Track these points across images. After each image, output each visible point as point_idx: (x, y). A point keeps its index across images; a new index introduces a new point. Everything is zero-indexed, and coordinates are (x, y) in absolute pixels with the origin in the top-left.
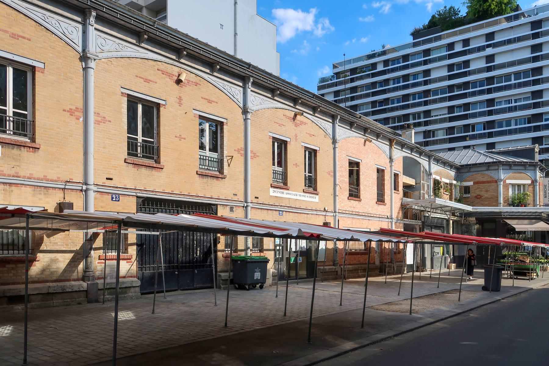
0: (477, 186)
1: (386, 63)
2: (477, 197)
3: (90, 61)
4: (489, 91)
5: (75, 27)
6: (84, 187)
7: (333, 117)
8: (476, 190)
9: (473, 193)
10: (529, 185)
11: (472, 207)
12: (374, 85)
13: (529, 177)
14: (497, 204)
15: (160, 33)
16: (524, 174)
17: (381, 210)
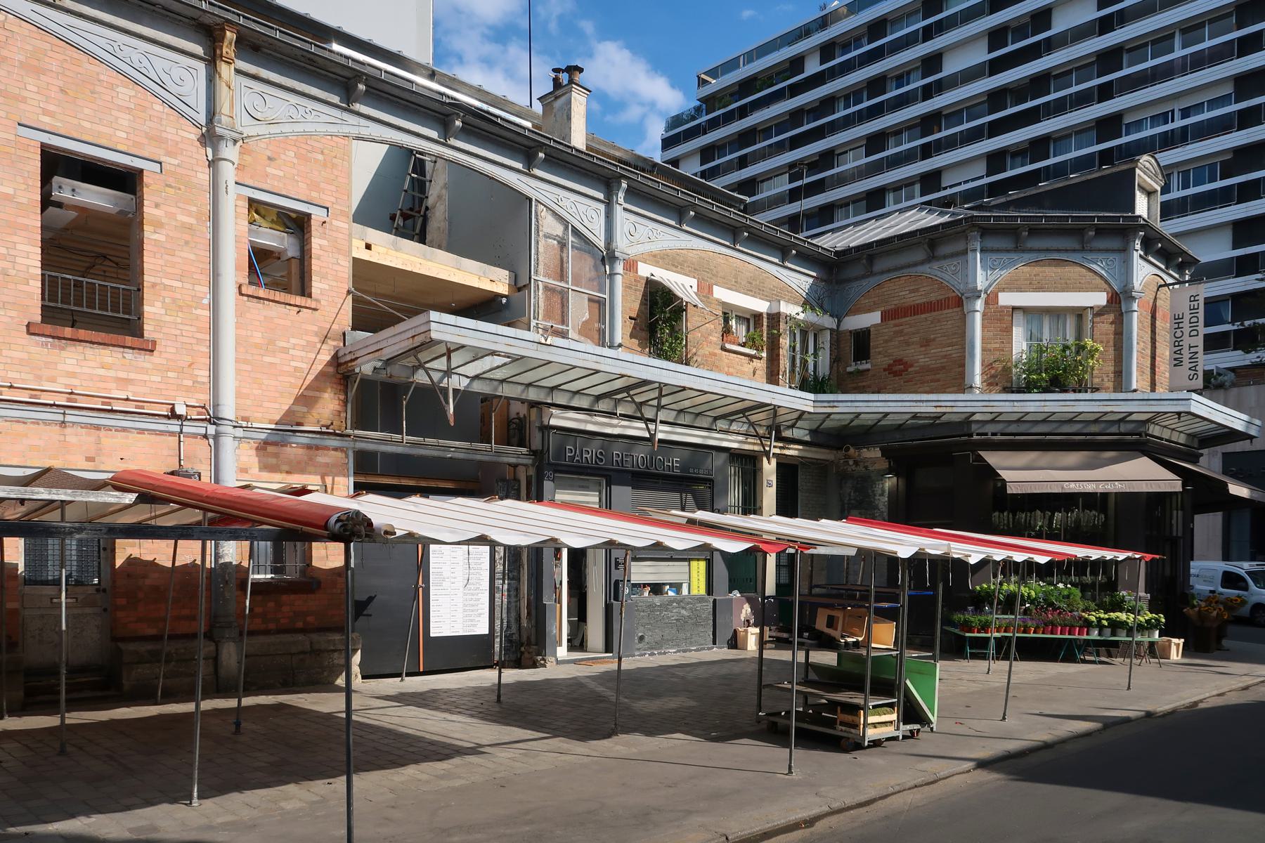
0: (896, 325)
1: (827, 51)
3: (223, 144)
4: (1105, 93)
5: (145, 53)
6: (212, 430)
7: (209, 34)
8: (889, 344)
9: (880, 353)
10: (1099, 312)
11: (811, 396)
12: (796, 116)
13: (1098, 281)
14: (961, 384)
15: (766, 228)
16: (1078, 269)
17: (112, 373)
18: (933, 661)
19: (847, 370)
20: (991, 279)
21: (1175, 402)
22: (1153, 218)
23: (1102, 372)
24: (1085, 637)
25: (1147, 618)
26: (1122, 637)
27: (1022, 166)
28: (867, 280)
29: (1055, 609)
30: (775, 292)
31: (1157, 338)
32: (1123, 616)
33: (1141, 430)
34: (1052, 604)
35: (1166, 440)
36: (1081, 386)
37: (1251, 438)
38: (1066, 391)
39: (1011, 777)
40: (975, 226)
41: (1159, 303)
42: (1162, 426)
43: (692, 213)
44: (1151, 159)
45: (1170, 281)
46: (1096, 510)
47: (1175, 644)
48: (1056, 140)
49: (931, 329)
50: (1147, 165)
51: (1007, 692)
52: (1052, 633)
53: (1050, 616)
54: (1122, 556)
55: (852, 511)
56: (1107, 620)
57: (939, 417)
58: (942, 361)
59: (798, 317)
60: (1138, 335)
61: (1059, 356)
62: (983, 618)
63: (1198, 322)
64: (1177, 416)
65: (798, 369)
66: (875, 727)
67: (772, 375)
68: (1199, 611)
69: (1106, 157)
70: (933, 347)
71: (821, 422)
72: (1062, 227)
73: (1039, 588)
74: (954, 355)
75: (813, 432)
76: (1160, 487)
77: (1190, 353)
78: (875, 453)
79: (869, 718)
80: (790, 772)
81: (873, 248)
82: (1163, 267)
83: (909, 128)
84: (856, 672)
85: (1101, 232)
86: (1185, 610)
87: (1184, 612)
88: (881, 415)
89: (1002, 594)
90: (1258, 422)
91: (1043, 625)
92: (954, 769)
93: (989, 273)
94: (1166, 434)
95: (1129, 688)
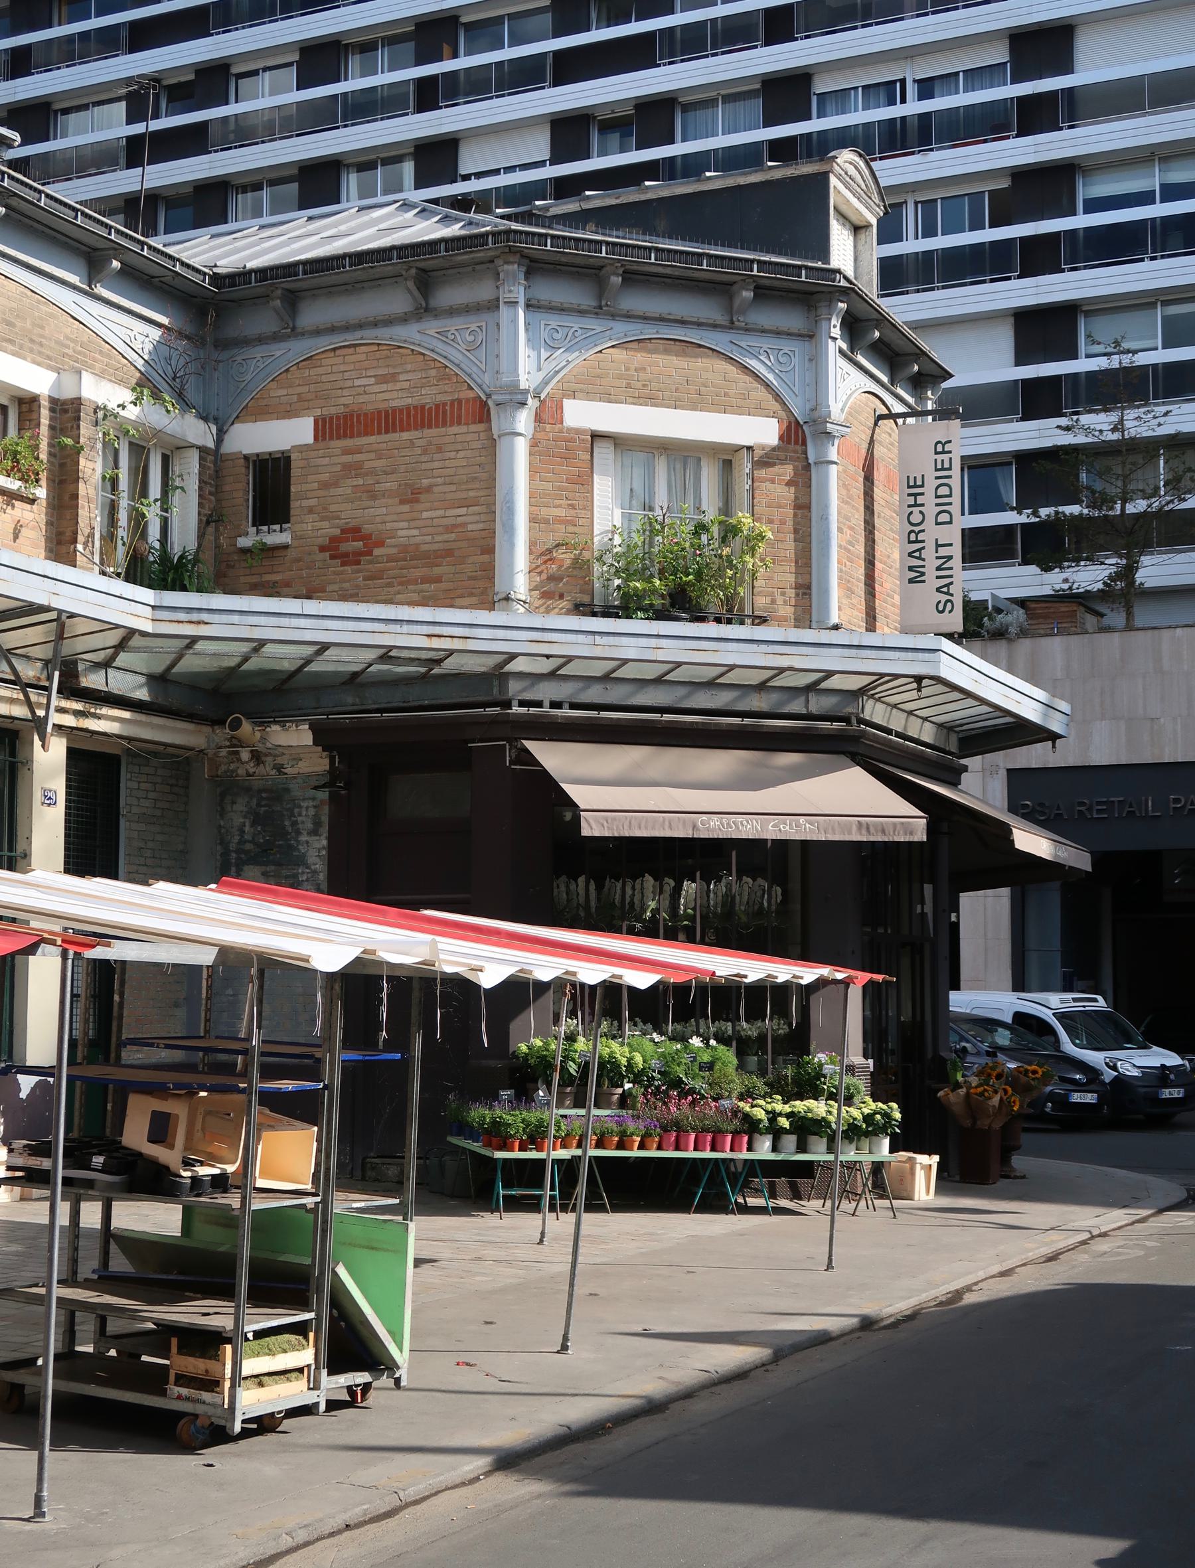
0: (347, 452)
2: (345, 547)
9: (311, 510)
10: (766, 459)
11: (147, 595)
13: (762, 394)
15: (48, 200)
18: (400, 1218)
19: (239, 545)
20: (548, 367)
21: (910, 655)
22: (866, 278)
23: (770, 583)
24: (745, 1155)
25: (866, 1111)
26: (818, 1153)
27: (622, 150)
28: (283, 345)
29: (683, 1094)
30: (70, 352)
31: (877, 522)
32: (818, 1108)
33: (850, 710)
34: (677, 1083)
35: (898, 735)
36: (730, 610)
37: (1053, 737)
38: (702, 619)
39: (568, 1488)
40: (515, 253)
41: (879, 451)
42: (888, 704)
43: (116, 264)
44: (857, 159)
45: (898, 408)
46: (765, 879)
47: (923, 1167)
48: (686, 108)
49: (424, 466)
50: (852, 170)
51: (572, 1285)
52: (677, 1148)
53: (673, 1109)
54: (808, 974)
55: (246, 868)
56: (789, 1116)
57: (439, 662)
58: (446, 537)
59: (122, 413)
60: (839, 513)
61: (687, 545)
62: (533, 1116)
63: (950, 496)
64: (915, 685)
65: (121, 533)
66: (261, 1385)
67: (59, 543)
68: (968, 1094)
69: (782, 150)
70: (428, 505)
71: (174, 656)
72: (689, 274)
73: (649, 1047)
74: (470, 527)
75: (157, 680)
76: (883, 832)
77: (937, 558)
78: (299, 736)
79: (244, 1362)
80: (39, 1513)
81: (296, 274)
82: (885, 379)
83: (391, 41)
84: (222, 1249)
85: (765, 293)
86: (941, 1094)
87: (939, 1099)
88: (310, 650)
89: (574, 1061)
90: (1064, 706)
91: (658, 1130)
92: (442, 1478)
93: (544, 354)
94: (897, 722)
95: (830, 1266)
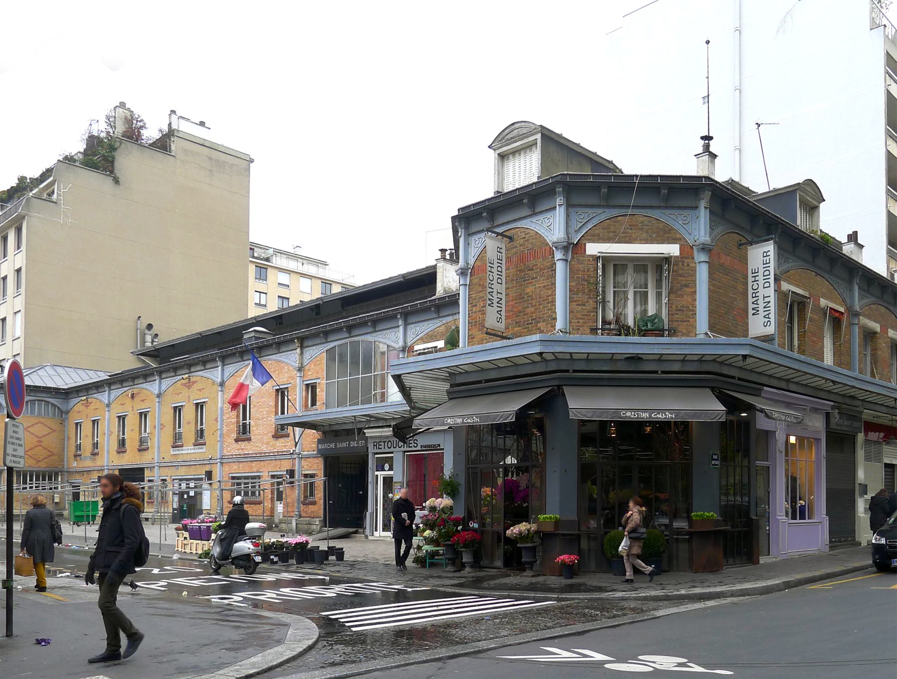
63: (769, 275)
